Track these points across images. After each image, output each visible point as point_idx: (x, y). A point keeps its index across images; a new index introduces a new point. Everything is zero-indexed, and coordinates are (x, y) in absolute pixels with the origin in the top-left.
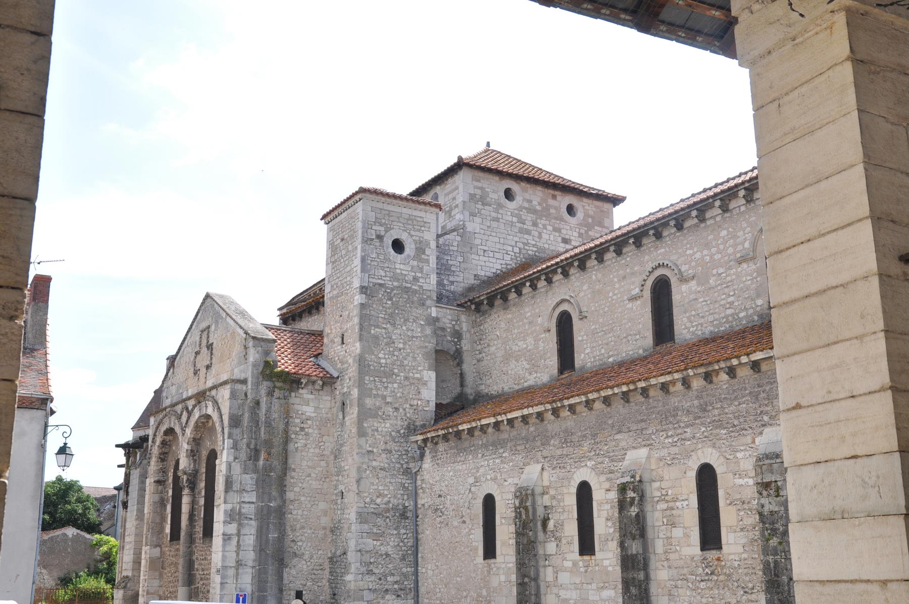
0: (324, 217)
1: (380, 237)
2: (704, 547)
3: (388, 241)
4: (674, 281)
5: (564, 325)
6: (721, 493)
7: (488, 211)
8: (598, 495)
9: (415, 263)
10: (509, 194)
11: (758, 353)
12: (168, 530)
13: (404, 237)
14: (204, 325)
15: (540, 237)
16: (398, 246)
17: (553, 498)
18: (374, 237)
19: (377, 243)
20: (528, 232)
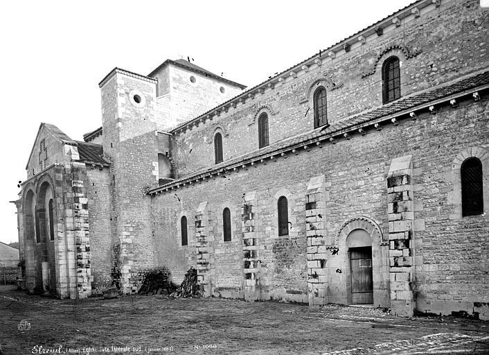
0: (101, 84)
1: (127, 93)
2: (280, 234)
3: (132, 97)
4: (269, 116)
5: (218, 138)
6: (289, 209)
7: (182, 87)
8: (233, 214)
9: (146, 108)
10: (192, 80)
11: (475, 76)
12: (35, 238)
13: (139, 94)
14: (40, 140)
15: (208, 102)
16: (137, 99)
17: (151, 115)
18: (124, 93)
19: (126, 96)
20: (202, 99)
